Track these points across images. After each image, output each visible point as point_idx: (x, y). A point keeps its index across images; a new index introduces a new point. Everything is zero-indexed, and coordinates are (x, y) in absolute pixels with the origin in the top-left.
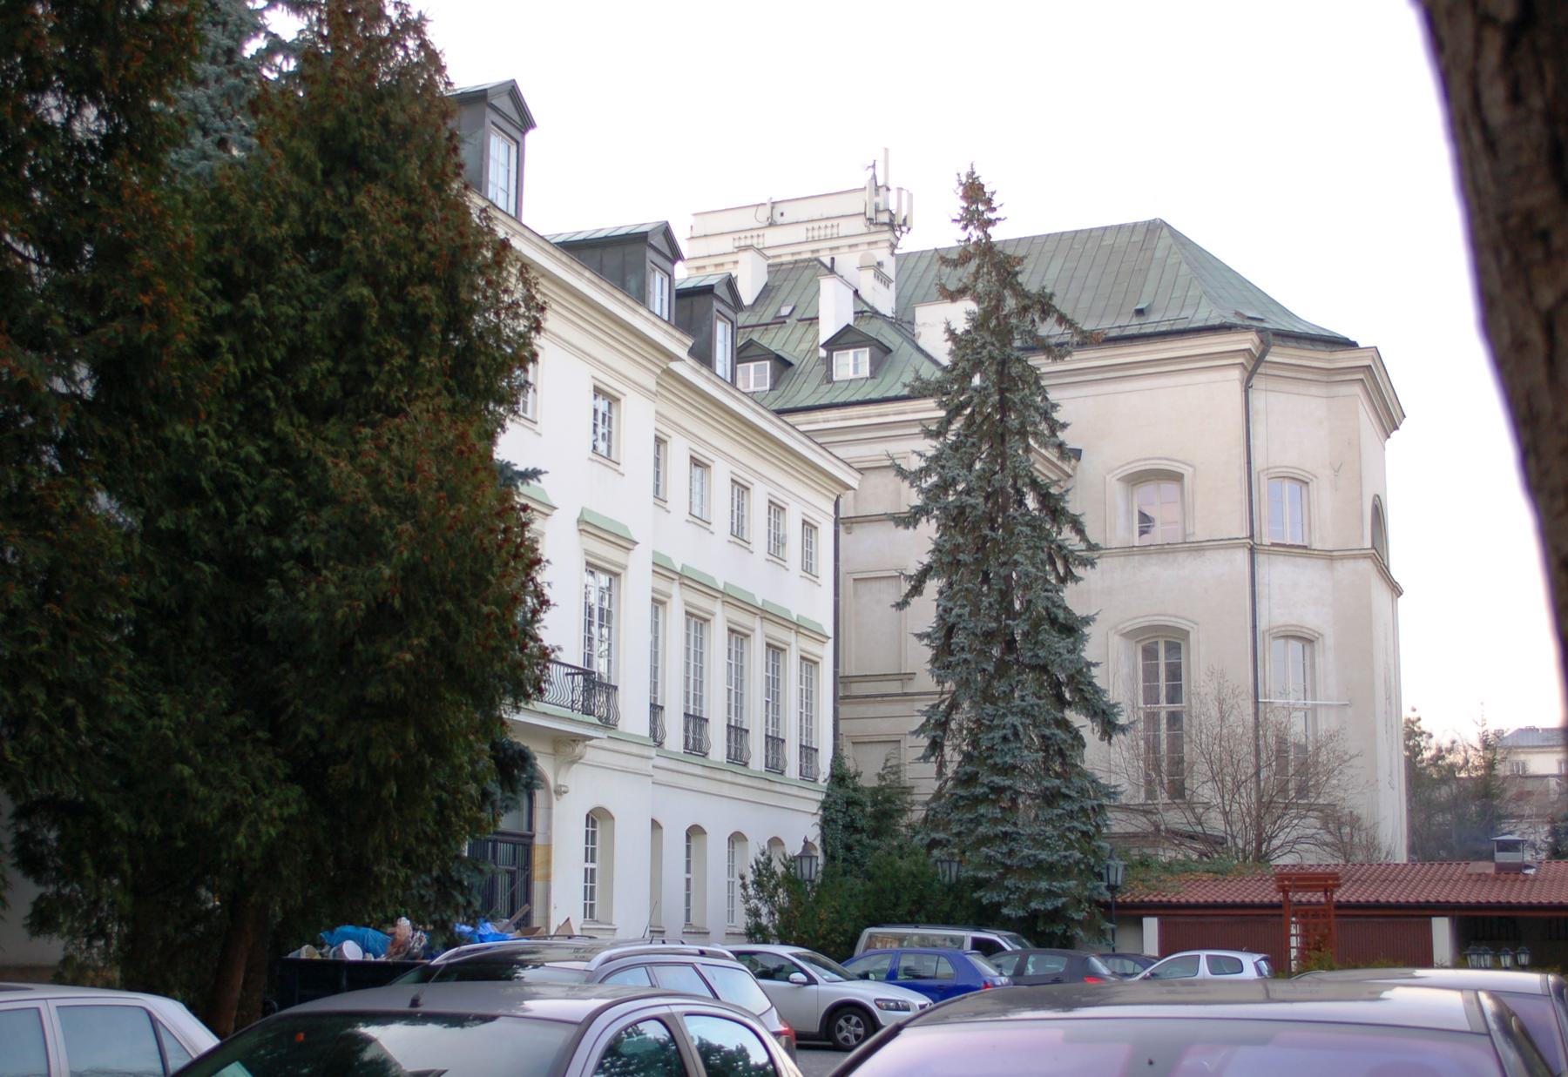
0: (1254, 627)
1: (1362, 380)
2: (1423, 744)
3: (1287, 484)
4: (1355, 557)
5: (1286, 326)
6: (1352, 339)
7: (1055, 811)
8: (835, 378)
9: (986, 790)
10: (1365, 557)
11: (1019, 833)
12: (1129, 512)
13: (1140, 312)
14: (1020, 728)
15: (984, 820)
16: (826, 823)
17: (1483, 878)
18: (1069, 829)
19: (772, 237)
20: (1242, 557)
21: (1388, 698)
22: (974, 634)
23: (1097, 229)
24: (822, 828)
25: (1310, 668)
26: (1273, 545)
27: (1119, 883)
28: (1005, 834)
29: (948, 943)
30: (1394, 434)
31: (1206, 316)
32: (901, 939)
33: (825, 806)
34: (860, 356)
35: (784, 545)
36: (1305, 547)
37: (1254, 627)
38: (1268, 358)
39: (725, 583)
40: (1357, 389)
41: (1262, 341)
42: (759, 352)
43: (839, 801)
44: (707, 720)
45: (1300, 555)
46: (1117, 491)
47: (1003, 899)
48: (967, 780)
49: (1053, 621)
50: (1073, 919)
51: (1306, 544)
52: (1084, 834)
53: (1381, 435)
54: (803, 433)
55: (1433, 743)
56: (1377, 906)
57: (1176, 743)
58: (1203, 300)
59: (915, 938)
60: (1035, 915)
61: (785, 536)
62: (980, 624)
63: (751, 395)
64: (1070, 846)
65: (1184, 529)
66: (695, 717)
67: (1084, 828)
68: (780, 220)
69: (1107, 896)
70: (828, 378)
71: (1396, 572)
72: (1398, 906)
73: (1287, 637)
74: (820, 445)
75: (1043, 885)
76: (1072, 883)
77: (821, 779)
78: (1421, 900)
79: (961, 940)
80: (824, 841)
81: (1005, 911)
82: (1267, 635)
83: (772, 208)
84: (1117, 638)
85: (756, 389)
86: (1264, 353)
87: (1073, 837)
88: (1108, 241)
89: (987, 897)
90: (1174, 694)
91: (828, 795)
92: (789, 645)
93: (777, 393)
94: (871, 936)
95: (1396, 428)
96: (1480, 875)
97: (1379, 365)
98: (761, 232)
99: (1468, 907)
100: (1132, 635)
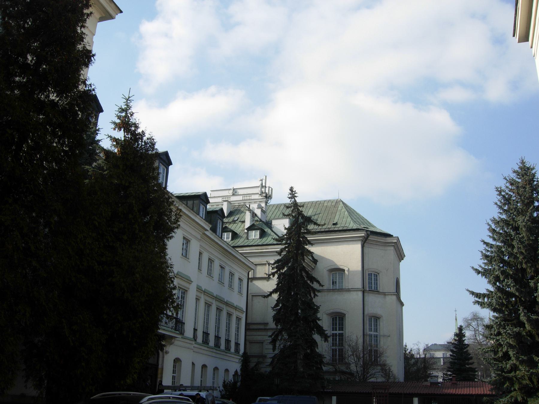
0: (364, 313)
8: (249, 238)
13: (334, 224)
20: (360, 294)
37: (364, 313)
38: (369, 238)
39: (236, 305)
92: (233, 313)
93: (232, 242)
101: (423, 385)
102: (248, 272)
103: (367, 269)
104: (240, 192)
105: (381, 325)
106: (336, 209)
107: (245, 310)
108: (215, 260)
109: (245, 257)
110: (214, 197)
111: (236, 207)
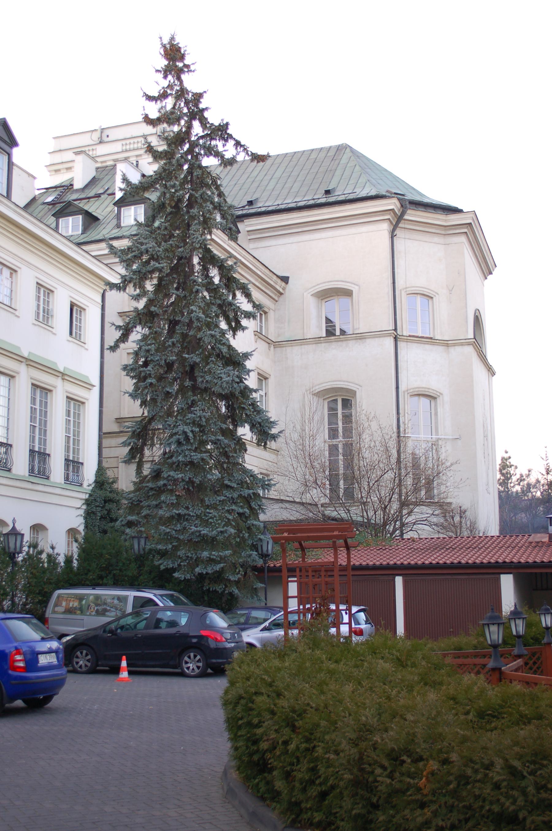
0: (397, 388)
1: (466, 233)
2: (512, 472)
3: (419, 298)
4: (462, 344)
5: (418, 198)
6: (460, 208)
7: (219, 498)
8: (122, 225)
9: (165, 482)
10: (469, 344)
11: (189, 515)
12: (319, 316)
13: (327, 192)
14: (190, 435)
15: (163, 505)
16: (89, 515)
17: (540, 545)
18: (228, 511)
19: (101, 150)
20: (390, 342)
21: (485, 436)
22: (159, 364)
23: (308, 151)
24: (85, 518)
25: (434, 415)
26: (410, 336)
27: (270, 552)
28: (179, 515)
29: (116, 602)
30: (490, 277)
31: (368, 192)
32: (80, 598)
33: (88, 502)
34: (138, 210)
35: (52, 316)
36: (431, 338)
37: (397, 388)
38: (406, 217)
39: (65, 368)
40: (463, 239)
41: (402, 206)
42: (75, 209)
43: (98, 499)
44: (82, 464)
45: (427, 343)
46: (311, 303)
47: (176, 565)
48: (157, 475)
49: (219, 356)
50: (230, 580)
51: (431, 336)
52: (240, 515)
53: (482, 277)
54: (94, 257)
55: (518, 472)
56: (459, 566)
57: (349, 465)
58: (367, 184)
59: (91, 598)
60: (201, 577)
61: (52, 310)
62: (164, 358)
63: (67, 238)
64: (228, 523)
65: (353, 326)
66: (73, 461)
67: (241, 511)
68: (105, 139)
69: (260, 562)
70: (118, 226)
71: (491, 360)
72: (474, 566)
73: (419, 395)
74: (106, 265)
75: (205, 554)
76: (228, 552)
77: (85, 484)
78: (500, 561)
79: (126, 598)
80: (86, 527)
81: (176, 575)
82: (406, 394)
83: (102, 132)
84: (310, 396)
85: (73, 234)
86: (403, 213)
87: (231, 517)
88: (313, 156)
89: (165, 564)
90: (348, 432)
91: (90, 495)
92: (55, 387)
93: (85, 235)
94: (58, 597)
95: (491, 273)
96: (538, 542)
97: (476, 222)
98: (94, 147)
99: (527, 565)
100: (321, 394)
101: (531, 543)
102: (102, 292)
103: (404, 289)
104: (114, 135)
105: (439, 414)
106: (337, 162)
107: (96, 381)
108: (56, 288)
109: (93, 256)
110: (60, 150)
111: (107, 168)
